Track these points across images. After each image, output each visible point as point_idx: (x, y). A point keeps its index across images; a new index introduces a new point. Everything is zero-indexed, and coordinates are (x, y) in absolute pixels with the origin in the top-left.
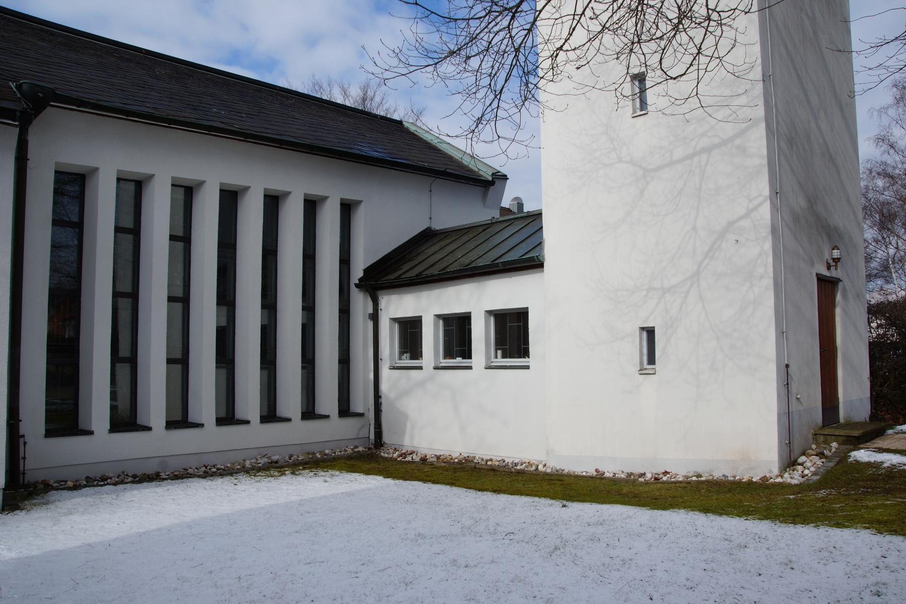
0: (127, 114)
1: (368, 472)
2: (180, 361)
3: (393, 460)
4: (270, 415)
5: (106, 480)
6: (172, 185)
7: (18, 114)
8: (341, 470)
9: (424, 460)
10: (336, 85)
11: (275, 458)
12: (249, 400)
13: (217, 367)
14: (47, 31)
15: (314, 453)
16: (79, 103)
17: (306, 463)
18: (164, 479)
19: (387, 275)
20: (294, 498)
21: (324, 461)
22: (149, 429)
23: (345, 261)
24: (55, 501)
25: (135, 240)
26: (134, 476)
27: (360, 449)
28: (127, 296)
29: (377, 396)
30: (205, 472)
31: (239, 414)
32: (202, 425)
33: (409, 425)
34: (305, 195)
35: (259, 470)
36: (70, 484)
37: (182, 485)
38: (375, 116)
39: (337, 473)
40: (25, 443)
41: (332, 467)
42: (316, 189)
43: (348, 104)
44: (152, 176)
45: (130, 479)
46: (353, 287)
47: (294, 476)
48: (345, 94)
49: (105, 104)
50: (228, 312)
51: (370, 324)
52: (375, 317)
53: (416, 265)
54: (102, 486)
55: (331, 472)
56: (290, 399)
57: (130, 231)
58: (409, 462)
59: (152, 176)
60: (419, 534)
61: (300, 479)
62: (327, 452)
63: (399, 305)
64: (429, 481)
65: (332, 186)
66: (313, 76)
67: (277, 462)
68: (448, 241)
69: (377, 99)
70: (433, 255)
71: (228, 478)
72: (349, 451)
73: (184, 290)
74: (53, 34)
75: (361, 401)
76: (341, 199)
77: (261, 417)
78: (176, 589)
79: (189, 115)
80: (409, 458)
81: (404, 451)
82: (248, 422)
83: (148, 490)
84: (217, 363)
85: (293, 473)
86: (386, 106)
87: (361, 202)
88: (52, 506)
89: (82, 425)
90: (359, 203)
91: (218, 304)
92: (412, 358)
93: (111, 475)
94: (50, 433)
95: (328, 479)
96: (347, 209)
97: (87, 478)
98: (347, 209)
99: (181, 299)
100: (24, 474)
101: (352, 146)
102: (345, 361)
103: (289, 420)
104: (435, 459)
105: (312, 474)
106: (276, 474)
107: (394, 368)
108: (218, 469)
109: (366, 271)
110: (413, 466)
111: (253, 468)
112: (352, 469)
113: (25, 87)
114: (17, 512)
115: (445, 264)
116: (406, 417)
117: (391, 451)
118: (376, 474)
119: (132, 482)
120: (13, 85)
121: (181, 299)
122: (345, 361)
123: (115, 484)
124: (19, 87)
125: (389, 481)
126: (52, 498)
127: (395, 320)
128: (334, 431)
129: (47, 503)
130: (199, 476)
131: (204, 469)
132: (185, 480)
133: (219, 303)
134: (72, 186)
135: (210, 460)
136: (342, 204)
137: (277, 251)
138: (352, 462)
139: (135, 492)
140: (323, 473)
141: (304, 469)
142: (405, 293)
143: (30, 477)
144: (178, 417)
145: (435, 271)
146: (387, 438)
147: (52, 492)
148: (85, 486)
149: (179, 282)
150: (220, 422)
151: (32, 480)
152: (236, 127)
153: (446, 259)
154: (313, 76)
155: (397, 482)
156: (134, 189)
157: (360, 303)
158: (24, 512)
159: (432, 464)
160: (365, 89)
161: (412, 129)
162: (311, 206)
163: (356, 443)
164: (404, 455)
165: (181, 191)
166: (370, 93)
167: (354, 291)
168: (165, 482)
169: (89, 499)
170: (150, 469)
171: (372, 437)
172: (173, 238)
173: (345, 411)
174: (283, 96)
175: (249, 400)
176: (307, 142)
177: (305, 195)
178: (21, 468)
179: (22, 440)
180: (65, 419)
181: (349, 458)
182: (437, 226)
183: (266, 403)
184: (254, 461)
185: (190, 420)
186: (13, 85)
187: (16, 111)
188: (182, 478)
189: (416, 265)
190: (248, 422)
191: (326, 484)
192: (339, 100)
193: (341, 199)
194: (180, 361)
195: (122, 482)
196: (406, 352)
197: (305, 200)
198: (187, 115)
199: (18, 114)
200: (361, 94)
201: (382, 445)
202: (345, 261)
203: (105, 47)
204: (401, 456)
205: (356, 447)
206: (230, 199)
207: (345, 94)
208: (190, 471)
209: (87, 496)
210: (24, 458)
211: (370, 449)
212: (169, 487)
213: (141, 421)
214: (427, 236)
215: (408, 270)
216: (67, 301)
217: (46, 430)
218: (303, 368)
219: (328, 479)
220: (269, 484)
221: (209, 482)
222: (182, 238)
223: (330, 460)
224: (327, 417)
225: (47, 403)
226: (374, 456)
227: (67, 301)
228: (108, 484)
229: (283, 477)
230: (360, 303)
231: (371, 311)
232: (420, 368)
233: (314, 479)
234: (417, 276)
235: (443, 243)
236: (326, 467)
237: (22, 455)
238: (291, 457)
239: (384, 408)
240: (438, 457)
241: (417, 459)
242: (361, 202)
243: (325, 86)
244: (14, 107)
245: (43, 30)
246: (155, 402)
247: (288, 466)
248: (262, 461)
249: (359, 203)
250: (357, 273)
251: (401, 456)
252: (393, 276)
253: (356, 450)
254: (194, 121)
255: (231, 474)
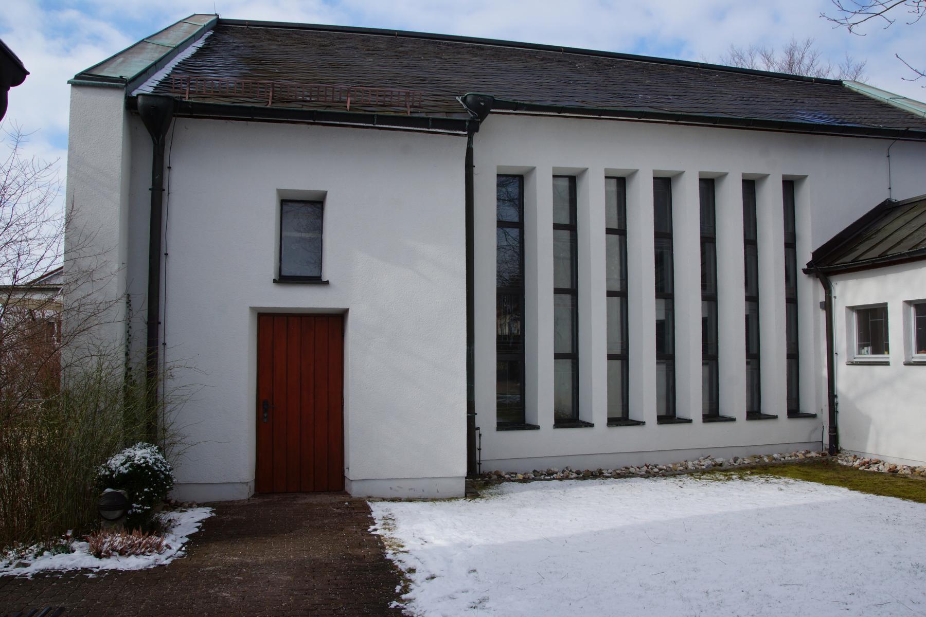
0: (559, 110)
1: (828, 482)
2: (620, 357)
3: (852, 468)
4: (713, 414)
5: (552, 474)
6: (554, 176)
7: (467, 124)
8: (794, 477)
9: (894, 471)
10: (758, 54)
11: (719, 460)
12: (691, 400)
13: (657, 363)
14: (477, 47)
15: (760, 457)
16: (515, 106)
17: (753, 468)
18: (607, 477)
19: (841, 256)
20: (750, 507)
21: (773, 466)
22: (591, 425)
23: (791, 244)
24: (508, 492)
25: (571, 236)
26: (578, 473)
27: (813, 454)
28: (569, 292)
29: (832, 396)
30: (646, 472)
31: (680, 412)
32: (644, 423)
33: (872, 428)
34: (743, 175)
35: (704, 472)
36: (520, 476)
37: (626, 484)
38: (809, 80)
39: (792, 481)
40: (480, 435)
41: (785, 474)
42: (754, 168)
43: (772, 70)
44: (533, 169)
45: (574, 475)
46: (800, 273)
47: (744, 482)
48: (768, 58)
49: (538, 103)
50: (666, 305)
51: (823, 314)
52: (827, 306)
53: (877, 244)
54: (548, 480)
55: (783, 479)
56: (734, 398)
57: (568, 228)
58: (874, 472)
59: (533, 169)
60: (918, 566)
61: (750, 485)
62: (775, 456)
63: (856, 291)
64: (909, 498)
65: (772, 161)
66: (732, 47)
67: (721, 465)
68: (916, 213)
69: (806, 61)
70: (896, 232)
71: (671, 480)
72: (801, 456)
73: (621, 284)
74: (482, 49)
75: (813, 398)
76: (783, 176)
77: (703, 415)
78: (640, 597)
79: (617, 104)
80: (874, 468)
81: (866, 460)
82: (690, 421)
83: (593, 488)
84: (657, 358)
85: (741, 478)
86: (817, 68)
87: (805, 177)
88: (506, 497)
89: (529, 420)
90: (802, 178)
91: (657, 297)
92: (874, 352)
93: (556, 470)
94: (501, 427)
95: (782, 487)
96: (790, 186)
97: (534, 471)
98: (790, 186)
99: (620, 294)
100: (480, 464)
101: (791, 115)
102: (793, 356)
103: (733, 420)
104: (908, 471)
105: (763, 480)
106: (722, 477)
107: (853, 364)
108: (660, 470)
109: (815, 254)
110: (881, 478)
111: (697, 470)
112: (808, 478)
113: (469, 99)
114: (478, 499)
115: (916, 241)
116: (868, 420)
117: (851, 458)
118: (839, 485)
119: (577, 478)
120: (459, 99)
121: (620, 294)
122: (793, 356)
123: (561, 479)
124: (464, 100)
125: (856, 494)
126: (505, 490)
127: (852, 308)
128: (782, 434)
129: (501, 494)
130: (642, 476)
131: (645, 468)
132: (628, 479)
133: (658, 296)
134: (513, 187)
135: (651, 460)
136: (784, 182)
137: (715, 238)
138: (805, 469)
139: (581, 489)
140: (775, 480)
141: (752, 474)
142: (862, 277)
143: (485, 468)
144: (618, 414)
145: (903, 249)
146: (844, 442)
147: (505, 484)
148: (534, 480)
149: (616, 276)
150: (662, 420)
151: (487, 471)
152: (666, 110)
153: (916, 234)
154: (732, 47)
155: (868, 495)
156: (570, 184)
157: (810, 291)
158: (483, 501)
159: (904, 477)
160: (791, 53)
161: (855, 87)
162: (709, 186)
163: (808, 447)
164: (868, 464)
165: (614, 182)
166: (797, 56)
167: (802, 278)
168: (609, 480)
169: (539, 493)
170: (593, 467)
171: (826, 441)
172: (609, 231)
173: (794, 411)
174: (708, 73)
175: (691, 400)
176: (743, 116)
177: (743, 175)
178: (478, 459)
179: (477, 432)
180: (513, 415)
181: (801, 464)
182: (899, 196)
183: (707, 402)
184: (696, 462)
185: (630, 418)
186: (459, 99)
187: (465, 121)
188: (625, 477)
189: (877, 244)
190: (690, 421)
191: (782, 493)
192: (761, 66)
193: (783, 176)
194: (620, 357)
195: (567, 478)
196: (867, 346)
197: (743, 181)
198: (615, 104)
199: (467, 124)
200: (787, 58)
201: (838, 452)
202: (791, 244)
203: (527, 52)
204: (863, 464)
205: (808, 452)
206: (664, 186)
207: (768, 58)
208: (632, 470)
209: (536, 489)
210: (480, 449)
211: (824, 455)
212: (614, 486)
213: (583, 417)
214: (887, 209)
215: (861, 251)
216: (512, 297)
217: (498, 424)
218: (747, 363)
219: (782, 487)
220: (717, 489)
221: (653, 483)
222: (618, 231)
223: (780, 466)
224: (775, 417)
225: (498, 398)
226: (827, 462)
227: (512, 297)
228: (554, 479)
229: (731, 482)
230: (810, 291)
231: (822, 298)
232: (887, 364)
233: (766, 486)
234: (880, 256)
235: (908, 217)
236: (777, 473)
237: (477, 446)
238: (736, 460)
239: (841, 408)
240: (913, 470)
241: (884, 469)
242: (805, 177)
243: (746, 55)
244: (463, 119)
245: (473, 47)
246: (596, 400)
247: (734, 470)
248: (707, 463)
249: (802, 178)
250: (805, 256)
251: (863, 464)
252: (849, 258)
253: (808, 455)
254: (624, 109)
255: (674, 475)
